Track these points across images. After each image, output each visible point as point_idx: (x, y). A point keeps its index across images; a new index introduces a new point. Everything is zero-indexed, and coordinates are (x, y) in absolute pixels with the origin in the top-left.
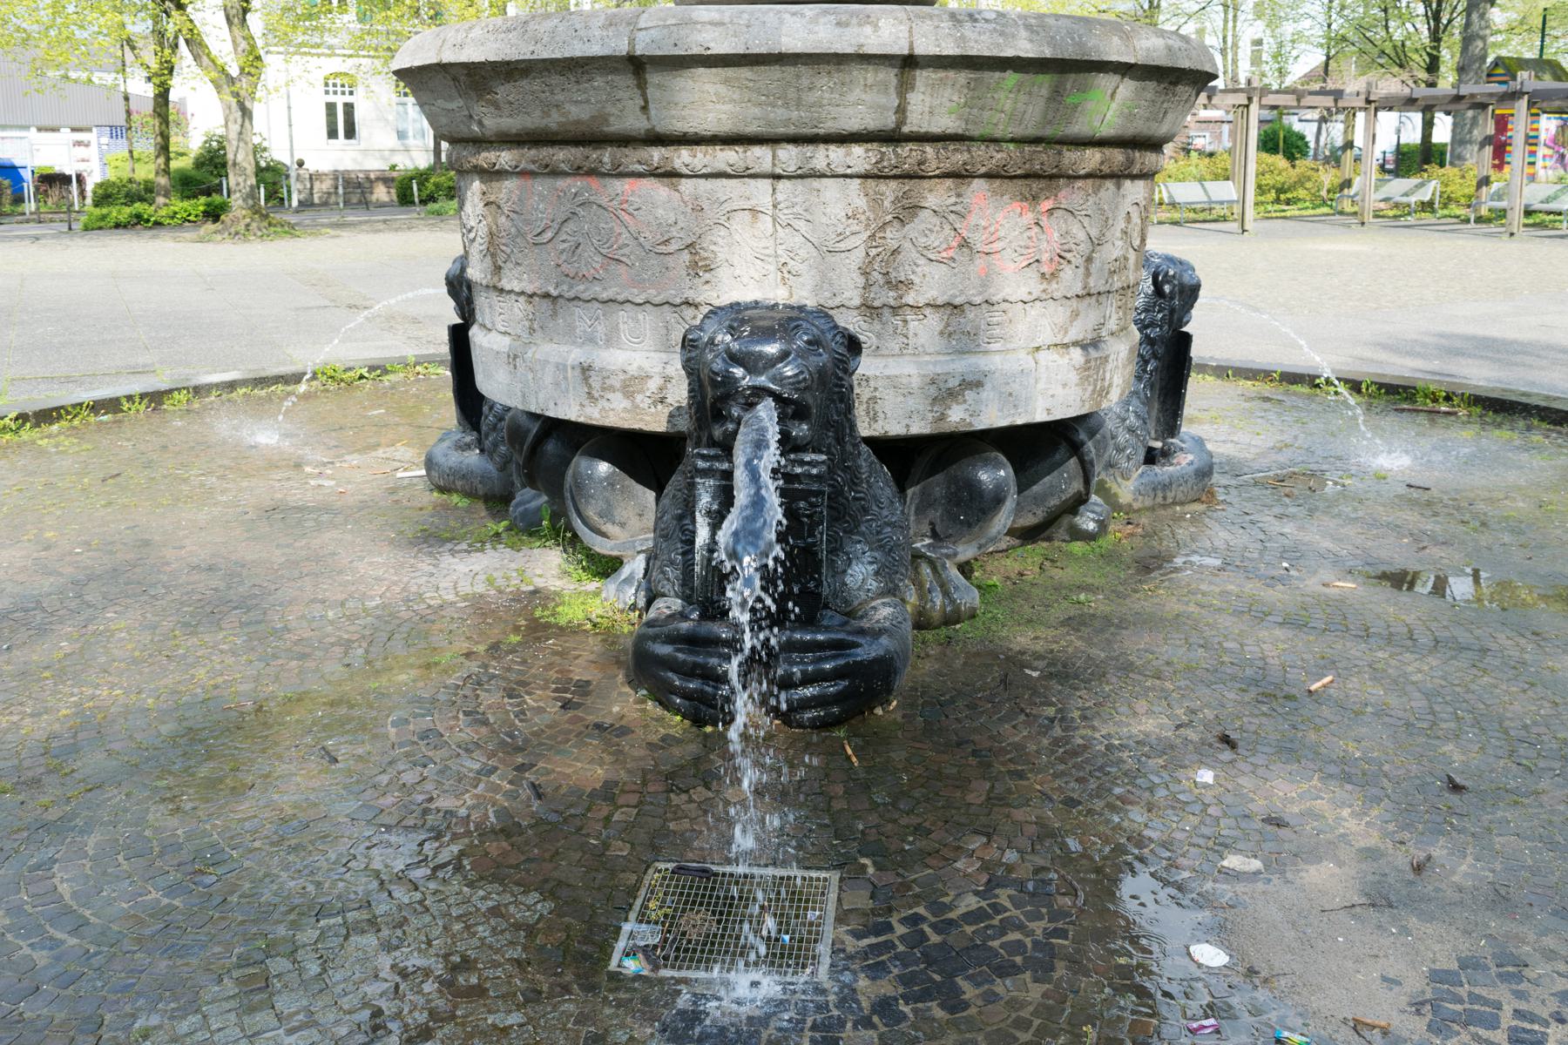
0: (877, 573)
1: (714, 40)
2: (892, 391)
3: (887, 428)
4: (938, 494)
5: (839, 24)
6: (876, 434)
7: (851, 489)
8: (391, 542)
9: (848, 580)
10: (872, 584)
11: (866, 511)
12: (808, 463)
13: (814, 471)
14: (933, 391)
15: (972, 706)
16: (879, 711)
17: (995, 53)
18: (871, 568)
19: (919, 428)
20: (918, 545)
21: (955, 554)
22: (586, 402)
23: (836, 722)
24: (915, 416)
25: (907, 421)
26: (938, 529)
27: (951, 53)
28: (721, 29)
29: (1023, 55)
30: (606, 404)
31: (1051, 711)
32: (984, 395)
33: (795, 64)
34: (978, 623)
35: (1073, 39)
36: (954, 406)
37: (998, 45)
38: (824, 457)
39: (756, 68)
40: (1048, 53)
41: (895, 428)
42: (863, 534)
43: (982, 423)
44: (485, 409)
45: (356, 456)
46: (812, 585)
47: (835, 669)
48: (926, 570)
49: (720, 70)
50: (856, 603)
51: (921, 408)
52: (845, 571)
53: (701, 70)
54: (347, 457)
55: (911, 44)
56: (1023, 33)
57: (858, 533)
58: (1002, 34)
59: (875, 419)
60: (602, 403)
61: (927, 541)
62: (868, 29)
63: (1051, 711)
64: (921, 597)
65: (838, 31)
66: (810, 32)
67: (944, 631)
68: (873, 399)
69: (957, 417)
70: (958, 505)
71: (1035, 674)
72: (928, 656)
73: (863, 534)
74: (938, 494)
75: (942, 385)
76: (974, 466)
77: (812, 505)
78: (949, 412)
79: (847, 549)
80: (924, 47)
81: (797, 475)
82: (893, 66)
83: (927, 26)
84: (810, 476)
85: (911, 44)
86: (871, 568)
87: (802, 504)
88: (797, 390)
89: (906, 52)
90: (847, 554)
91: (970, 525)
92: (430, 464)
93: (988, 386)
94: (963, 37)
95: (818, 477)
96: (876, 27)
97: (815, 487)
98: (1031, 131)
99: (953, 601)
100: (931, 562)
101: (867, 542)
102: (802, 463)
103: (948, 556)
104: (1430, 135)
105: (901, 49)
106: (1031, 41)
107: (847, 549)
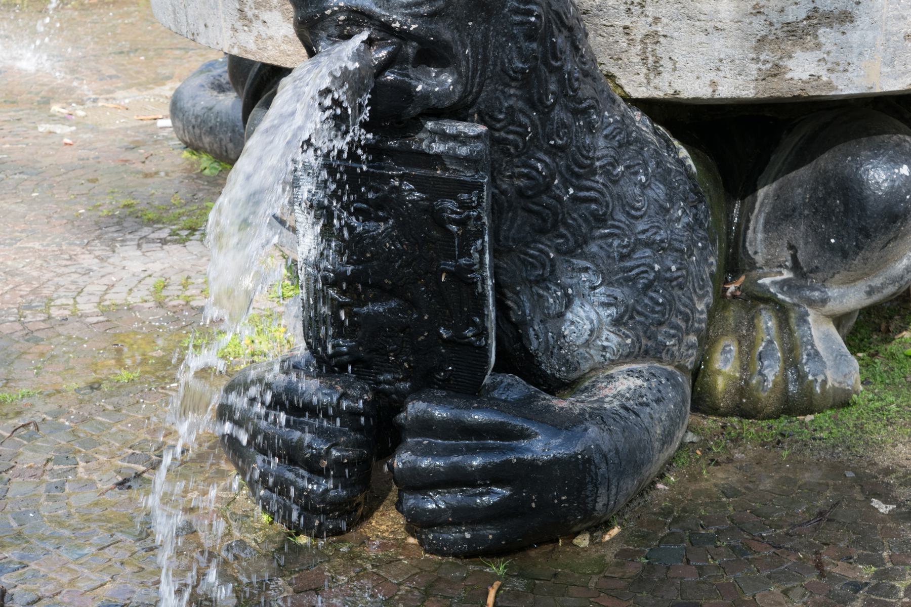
0: (617, 322)
2: (684, 24)
3: (678, 85)
4: (798, 200)
6: (659, 94)
7: (566, 184)
8: (73, 222)
9: (566, 329)
10: (611, 339)
11: (601, 220)
12: (455, 138)
13: (463, 151)
14: (758, 26)
15: (739, 551)
16: (583, 541)
18: (606, 314)
19: (735, 85)
20: (766, 281)
21: (824, 301)
22: (238, 25)
23: (493, 552)
24: (726, 68)
25: (712, 76)
26: (801, 257)
30: (262, 28)
31: (866, 573)
32: (854, 36)
34: (849, 417)
36: (799, 54)
38: (482, 129)
41: (692, 84)
42: (592, 258)
43: (849, 85)
45: (134, 91)
46: (469, 333)
47: (483, 469)
48: (767, 322)
50: (585, 367)
51: (737, 54)
52: (561, 315)
54: (119, 94)
57: (584, 256)
59: (656, 69)
60: (257, 26)
61: (787, 275)
63: (866, 573)
64: (745, 367)
67: (782, 424)
68: (652, 37)
69: (806, 72)
70: (827, 219)
71: (884, 509)
72: (730, 460)
73: (592, 258)
74: (798, 200)
75: (774, 17)
76: (855, 155)
77: (464, 206)
78: (790, 64)
79: (564, 280)
81: (438, 157)
84: (457, 158)
86: (605, 313)
87: (450, 204)
88: (415, 17)
90: (564, 288)
91: (845, 255)
92: (176, 109)
93: (863, 21)
95: (470, 162)
97: (467, 175)
99: (801, 377)
100: (782, 312)
101: (598, 271)
102: (445, 137)
103: (811, 303)
107: (564, 280)
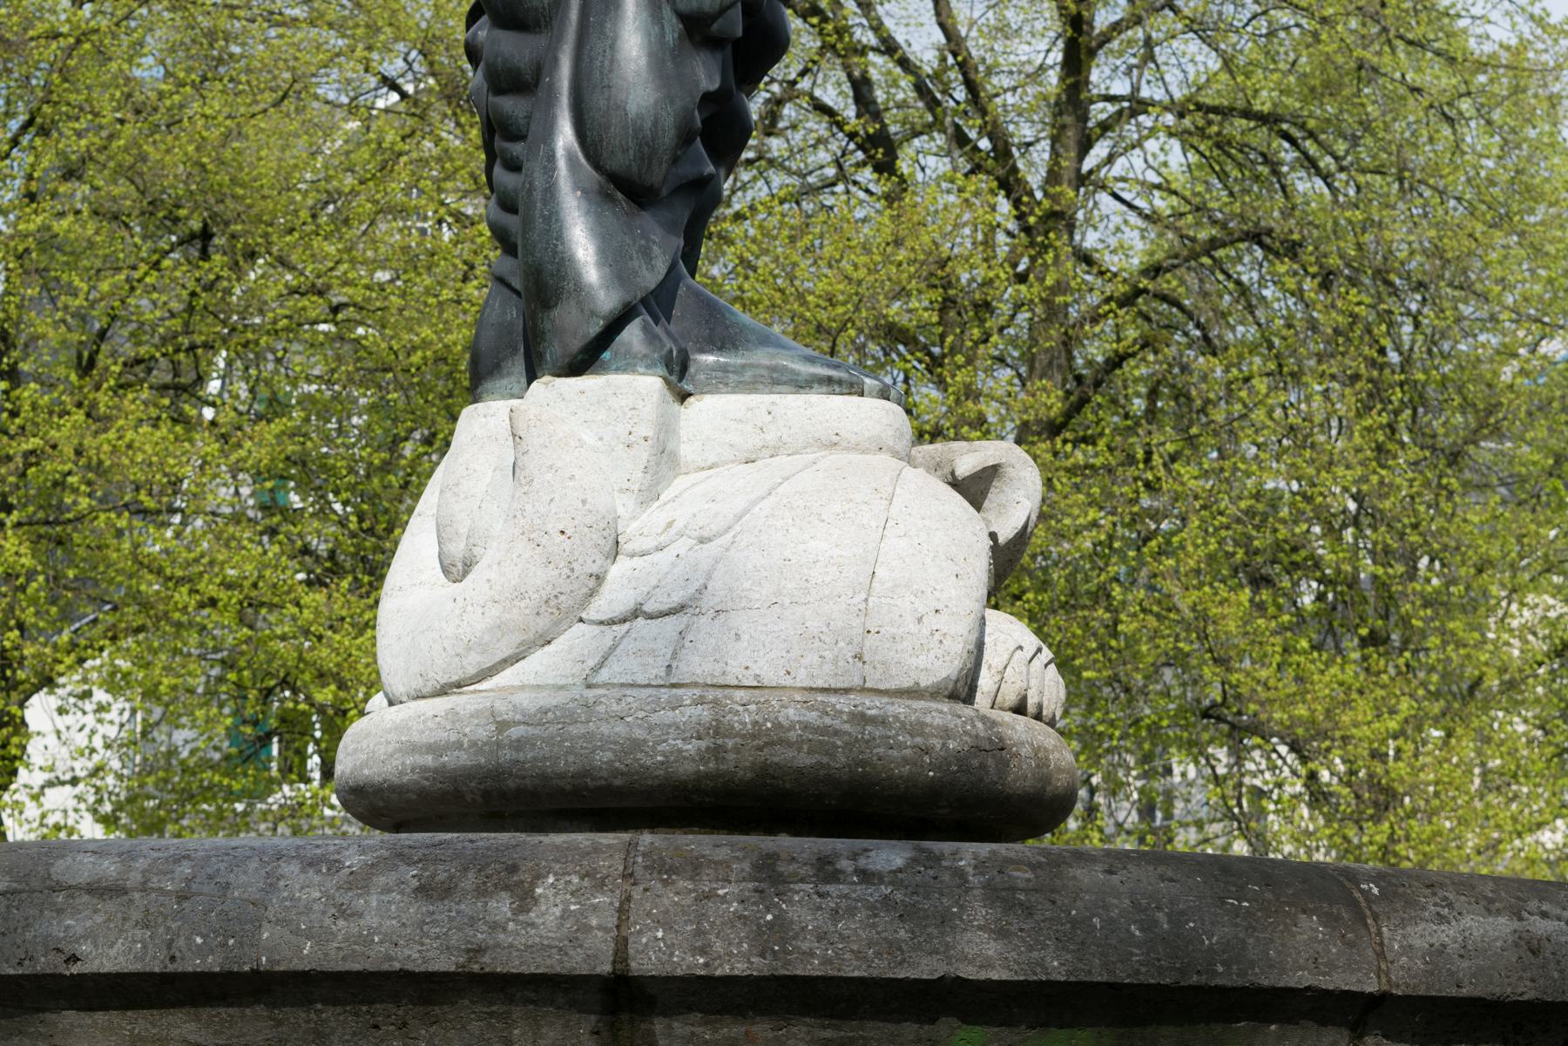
1: (90, 935)
5: (424, 891)
17: (881, 968)
27: (741, 969)
28: (111, 906)
29: (969, 972)
33: (307, 1002)
35: (1149, 926)
37: (893, 946)
39: (205, 1013)
40: (1056, 967)
44: (1072, 979)
49: (114, 1016)
53: (70, 1017)
55: (621, 945)
56: (980, 912)
58: (907, 914)
62: (502, 906)
65: (416, 910)
66: (343, 912)
80: (659, 951)
82: (583, 1009)
83: (674, 896)
85: (621, 945)
89: (605, 968)
94: (781, 923)
96: (525, 900)
98: (820, 683)
104: (669, 1012)
105: (593, 956)
106: (1002, 934)
